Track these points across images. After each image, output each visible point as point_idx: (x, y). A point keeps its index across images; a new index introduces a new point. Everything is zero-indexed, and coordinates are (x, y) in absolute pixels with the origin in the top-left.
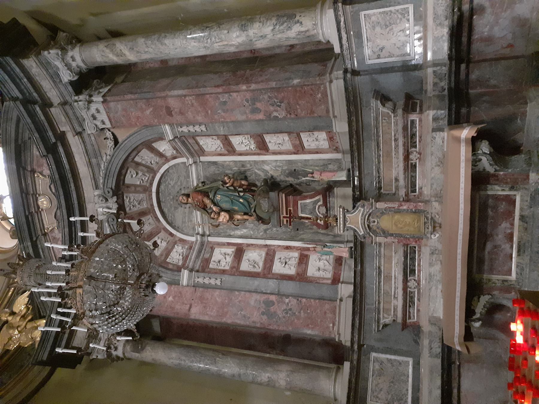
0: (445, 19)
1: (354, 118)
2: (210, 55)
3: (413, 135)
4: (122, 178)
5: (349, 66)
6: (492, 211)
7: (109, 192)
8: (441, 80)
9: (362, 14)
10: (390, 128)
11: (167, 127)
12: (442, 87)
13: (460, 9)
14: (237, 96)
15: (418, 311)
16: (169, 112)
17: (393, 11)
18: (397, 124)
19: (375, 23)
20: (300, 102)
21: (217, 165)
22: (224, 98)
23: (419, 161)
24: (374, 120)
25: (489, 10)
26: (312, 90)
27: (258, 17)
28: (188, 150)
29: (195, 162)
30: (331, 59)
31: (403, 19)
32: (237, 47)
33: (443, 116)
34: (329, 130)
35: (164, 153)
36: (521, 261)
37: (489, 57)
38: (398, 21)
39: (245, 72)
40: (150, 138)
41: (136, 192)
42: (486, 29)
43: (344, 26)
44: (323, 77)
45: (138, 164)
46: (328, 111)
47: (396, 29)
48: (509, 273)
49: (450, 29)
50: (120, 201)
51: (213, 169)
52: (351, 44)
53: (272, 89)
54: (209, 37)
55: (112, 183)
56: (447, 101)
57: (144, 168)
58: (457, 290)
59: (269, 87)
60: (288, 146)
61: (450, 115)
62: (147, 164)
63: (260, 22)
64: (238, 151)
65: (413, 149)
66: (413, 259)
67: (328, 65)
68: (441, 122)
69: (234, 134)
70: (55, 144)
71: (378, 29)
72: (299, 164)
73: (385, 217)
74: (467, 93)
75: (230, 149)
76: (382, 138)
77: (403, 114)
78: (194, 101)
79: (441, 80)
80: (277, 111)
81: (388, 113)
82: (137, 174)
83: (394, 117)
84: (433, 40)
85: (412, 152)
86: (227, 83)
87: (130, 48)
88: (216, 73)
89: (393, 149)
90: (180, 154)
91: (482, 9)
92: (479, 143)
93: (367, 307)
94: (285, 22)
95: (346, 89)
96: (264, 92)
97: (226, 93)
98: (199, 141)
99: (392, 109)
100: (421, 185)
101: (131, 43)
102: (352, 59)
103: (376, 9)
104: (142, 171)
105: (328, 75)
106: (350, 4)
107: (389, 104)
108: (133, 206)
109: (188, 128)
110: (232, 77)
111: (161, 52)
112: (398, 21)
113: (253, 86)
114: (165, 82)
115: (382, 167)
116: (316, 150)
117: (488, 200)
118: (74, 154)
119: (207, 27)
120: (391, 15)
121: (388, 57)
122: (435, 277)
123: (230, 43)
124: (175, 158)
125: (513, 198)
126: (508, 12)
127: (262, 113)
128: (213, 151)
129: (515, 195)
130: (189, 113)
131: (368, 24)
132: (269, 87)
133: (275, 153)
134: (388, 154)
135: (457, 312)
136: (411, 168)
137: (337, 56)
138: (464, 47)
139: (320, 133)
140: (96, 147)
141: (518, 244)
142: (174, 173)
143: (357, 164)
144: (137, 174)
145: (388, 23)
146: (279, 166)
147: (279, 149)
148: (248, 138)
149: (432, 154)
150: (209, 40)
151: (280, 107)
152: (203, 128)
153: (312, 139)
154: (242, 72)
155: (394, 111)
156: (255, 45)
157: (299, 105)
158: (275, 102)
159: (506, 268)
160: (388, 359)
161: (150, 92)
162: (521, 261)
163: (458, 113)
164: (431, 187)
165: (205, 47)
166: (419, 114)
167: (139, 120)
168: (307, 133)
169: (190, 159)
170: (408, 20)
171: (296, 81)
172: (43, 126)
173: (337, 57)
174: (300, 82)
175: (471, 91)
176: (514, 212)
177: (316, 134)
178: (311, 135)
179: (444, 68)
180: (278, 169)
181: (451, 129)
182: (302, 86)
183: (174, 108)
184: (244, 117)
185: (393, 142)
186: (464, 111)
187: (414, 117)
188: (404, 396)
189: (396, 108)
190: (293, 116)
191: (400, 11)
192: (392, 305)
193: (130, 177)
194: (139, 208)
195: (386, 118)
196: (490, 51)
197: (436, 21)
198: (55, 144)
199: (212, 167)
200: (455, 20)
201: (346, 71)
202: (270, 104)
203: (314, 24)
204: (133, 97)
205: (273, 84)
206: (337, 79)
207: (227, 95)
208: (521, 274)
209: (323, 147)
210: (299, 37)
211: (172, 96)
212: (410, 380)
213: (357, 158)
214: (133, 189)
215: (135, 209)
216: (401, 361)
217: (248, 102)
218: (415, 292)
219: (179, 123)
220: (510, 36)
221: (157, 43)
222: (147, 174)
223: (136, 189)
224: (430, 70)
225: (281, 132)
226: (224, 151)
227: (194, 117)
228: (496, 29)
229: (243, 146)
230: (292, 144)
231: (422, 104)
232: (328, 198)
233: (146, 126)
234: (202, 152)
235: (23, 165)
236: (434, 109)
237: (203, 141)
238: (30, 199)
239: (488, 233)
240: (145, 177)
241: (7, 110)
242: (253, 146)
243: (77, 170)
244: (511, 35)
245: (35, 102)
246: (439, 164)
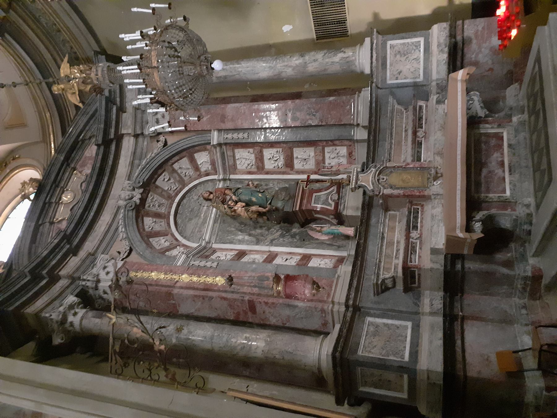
3: (420, 118)
4: (156, 176)
6: (485, 145)
7: (139, 183)
9: (389, 43)
10: (402, 122)
15: (420, 257)
18: (408, 118)
19: (397, 52)
23: (425, 139)
24: (390, 112)
25: (474, 41)
36: (513, 179)
38: (413, 51)
41: (161, 195)
42: (473, 56)
45: (174, 171)
48: (504, 191)
50: (145, 195)
55: (146, 176)
57: (177, 177)
58: (458, 184)
62: (181, 175)
66: (416, 218)
70: (112, 140)
73: (394, 175)
75: (260, 165)
80: (310, 119)
81: (401, 110)
82: (169, 180)
85: (418, 131)
91: (470, 40)
93: (366, 277)
100: (425, 159)
104: (175, 178)
108: (153, 206)
112: (413, 51)
115: (393, 153)
117: (481, 137)
118: (121, 156)
122: (437, 217)
124: (207, 175)
125: (501, 135)
127: (299, 121)
129: (502, 133)
130: (239, 120)
131: (392, 52)
134: (399, 143)
135: (458, 204)
136: (418, 144)
140: (145, 151)
141: (509, 166)
143: (372, 155)
144: (169, 180)
145: (405, 53)
147: (303, 168)
149: (435, 121)
157: (331, 115)
159: (501, 188)
160: (384, 323)
162: (513, 179)
164: (434, 146)
170: (420, 51)
172: (111, 123)
176: (503, 145)
185: (404, 133)
188: (401, 351)
192: (393, 264)
193: (162, 179)
194: (157, 209)
198: (112, 140)
208: (514, 189)
210: (341, 61)
212: (409, 339)
214: (160, 191)
215: (154, 209)
216: (399, 326)
218: (417, 243)
220: (490, 62)
222: (177, 184)
223: (162, 193)
227: (242, 124)
228: (480, 56)
232: (341, 188)
235: (69, 161)
238: (56, 191)
239: (483, 161)
240: (174, 186)
241: (90, 103)
243: (111, 187)
244: (491, 61)
245: (115, 104)
246: (441, 128)
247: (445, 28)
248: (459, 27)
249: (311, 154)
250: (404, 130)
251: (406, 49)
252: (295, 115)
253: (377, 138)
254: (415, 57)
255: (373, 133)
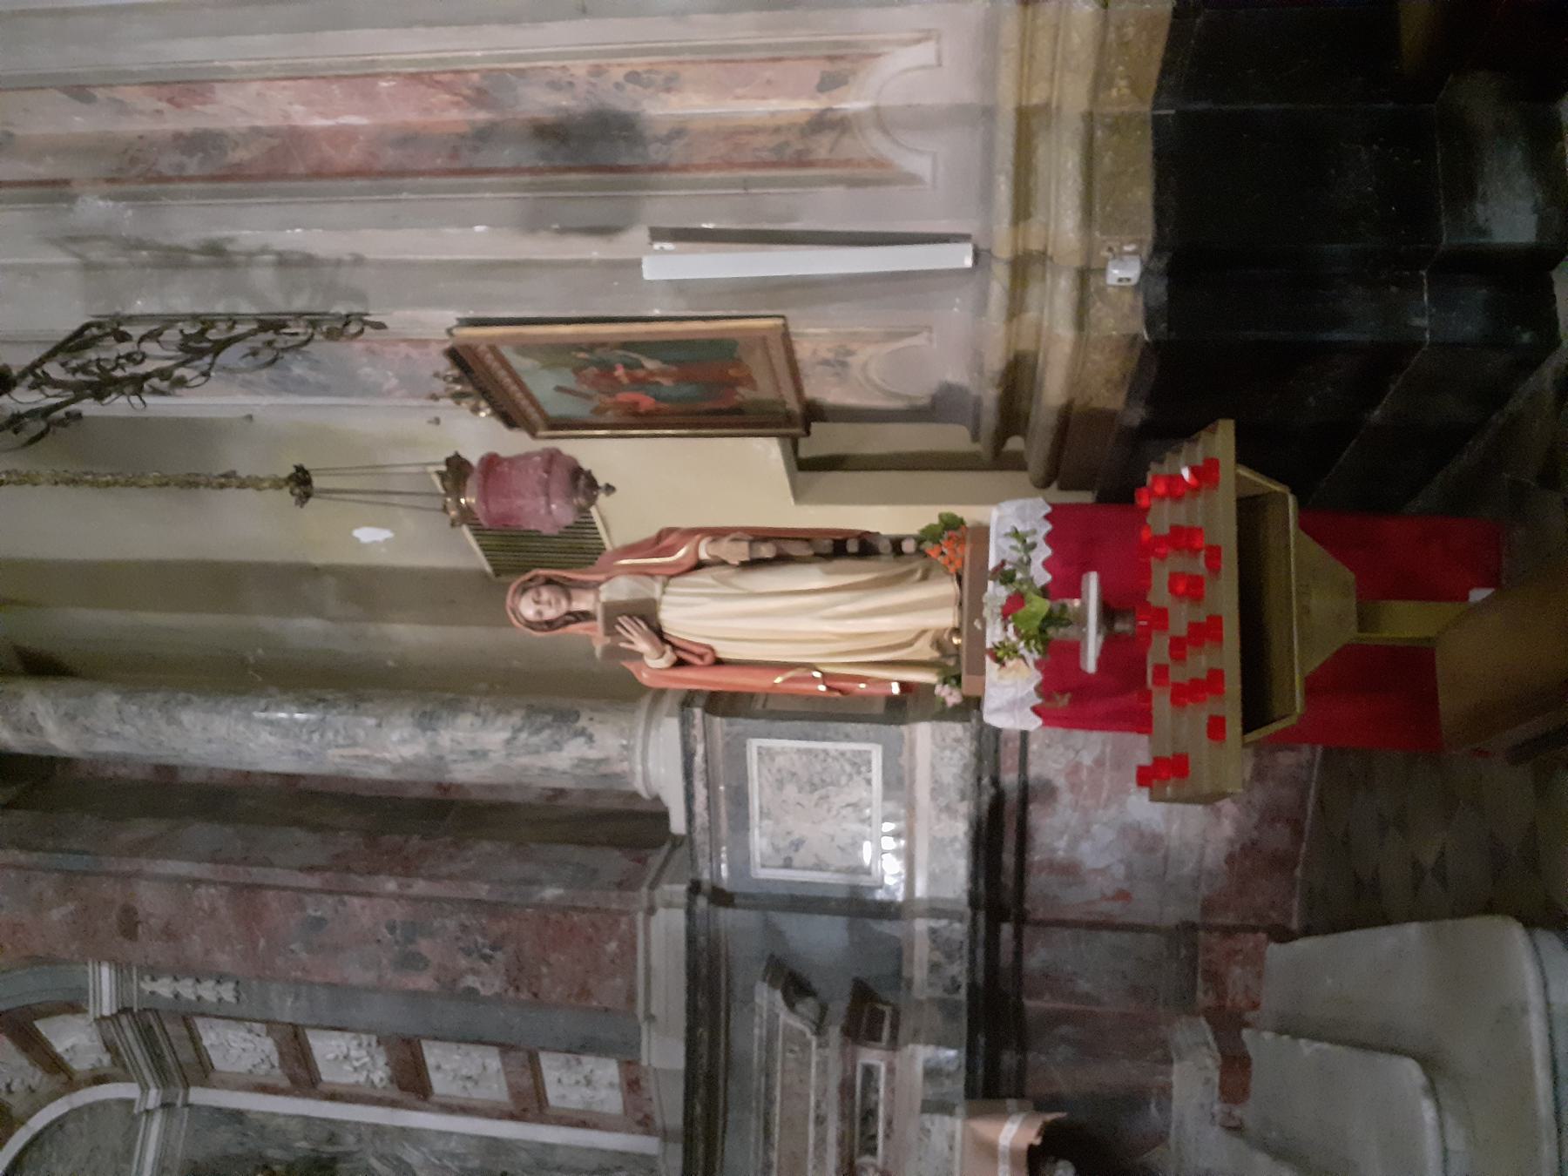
0: (958, 797)
1: (703, 1033)
2: (314, 777)
3: (869, 1115)
5: (706, 876)
8: (950, 957)
9: (754, 745)
10: (804, 1081)
11: (105, 972)
12: (953, 979)
13: (995, 782)
14: (363, 907)
16: (129, 924)
17: (833, 753)
20: (553, 958)
21: (241, 1122)
22: (320, 908)
24: (760, 1045)
25: (1065, 798)
26: (593, 925)
27: (473, 699)
28: (156, 1058)
29: (166, 1106)
30: (662, 843)
31: (856, 778)
32: (396, 768)
33: (952, 1068)
34: (629, 1058)
35: (66, 1057)
37: (1071, 916)
38: (844, 780)
39: (406, 841)
40: (33, 1000)
43: (704, 766)
44: (631, 894)
46: (631, 998)
47: (838, 800)
49: (971, 826)
51: (223, 1140)
52: (718, 815)
53: (477, 903)
54: (321, 726)
56: (965, 1021)
59: (468, 895)
60: (496, 1090)
61: (970, 1068)
63: (477, 714)
64: (331, 1083)
65: (867, 1159)
67: (650, 860)
68: (947, 1082)
69: (326, 1024)
71: (791, 790)
72: (523, 1155)
74: (1019, 1009)
75: (302, 1073)
76: (782, 1110)
77: (844, 1045)
78: (221, 903)
79: (950, 957)
81: (803, 1034)
83: (820, 1046)
84: (930, 845)
86: (341, 864)
87: (66, 714)
88: (317, 828)
89: (811, 1149)
90: (124, 1066)
91: (1049, 792)
92: (1048, 1166)
94: (548, 726)
95: (691, 940)
96: (448, 907)
97: (330, 892)
98: (202, 1032)
99: (814, 1023)
101: (72, 702)
102: (714, 858)
103: (790, 739)
105: (644, 890)
106: (724, 715)
107: (808, 1006)
109: (176, 984)
110: (362, 847)
111: (160, 744)
113: (420, 887)
114: (146, 828)
116: (582, 1117)
119: (320, 700)
120: (825, 761)
121: (811, 869)
123: (378, 755)
124: (99, 1079)
126: (1113, 810)
128: (239, 1073)
131: (765, 772)
132: (466, 897)
133: (449, 1108)
137: (677, 842)
138: (1008, 880)
139: (603, 1061)
142: (81, 1134)
145: (816, 780)
146: (453, 1156)
147: (465, 1095)
148: (369, 1045)
150: (316, 737)
151: (489, 963)
152: (227, 992)
153: (574, 1078)
154: (397, 838)
155: (820, 1028)
156: (450, 772)
157: (549, 965)
158: (476, 942)
161: (85, 852)
163: (993, 1064)
165: (299, 752)
166: (887, 1049)
167: (19, 935)
168: (562, 1057)
169: (153, 1092)
170: (869, 782)
171: (551, 893)
173: (678, 843)
174: (560, 898)
175: (1029, 1003)
177: (589, 1062)
178: (573, 1063)
179: (957, 925)
180: (450, 1164)
181: (972, 1114)
182: (566, 910)
183: (150, 915)
184: (369, 977)
185: (811, 1127)
186: (1008, 1059)
187: (872, 1056)
189: (826, 1022)
190: (525, 995)
191: (848, 755)
195: (797, 1048)
196: (1073, 901)
197: (936, 800)
199: (223, 1127)
200: (985, 807)
201: (695, 888)
202: (462, 949)
203: (624, 747)
204: (22, 857)
205: (482, 891)
206: (669, 905)
207: (330, 900)
209: (606, 1109)
210: (578, 771)
211: (156, 877)
213: (701, 1163)
217: (392, 928)
219: (150, 962)
220: (1119, 871)
221: (157, 714)
224: (921, 925)
225: (480, 1042)
226: (279, 1078)
227: (207, 952)
228: (1085, 847)
229: (347, 1067)
230: (510, 1086)
231: (898, 1019)
233: (34, 960)
234: (202, 1071)
236: (927, 1043)
237: (212, 1036)
242: (380, 1074)
247: (958, 740)
248: (1010, 745)
249: (488, 1061)
250: (812, 1115)
251: (818, 768)
252: (411, 947)
253: (721, 1101)
254: (853, 799)
255: (702, 1091)
